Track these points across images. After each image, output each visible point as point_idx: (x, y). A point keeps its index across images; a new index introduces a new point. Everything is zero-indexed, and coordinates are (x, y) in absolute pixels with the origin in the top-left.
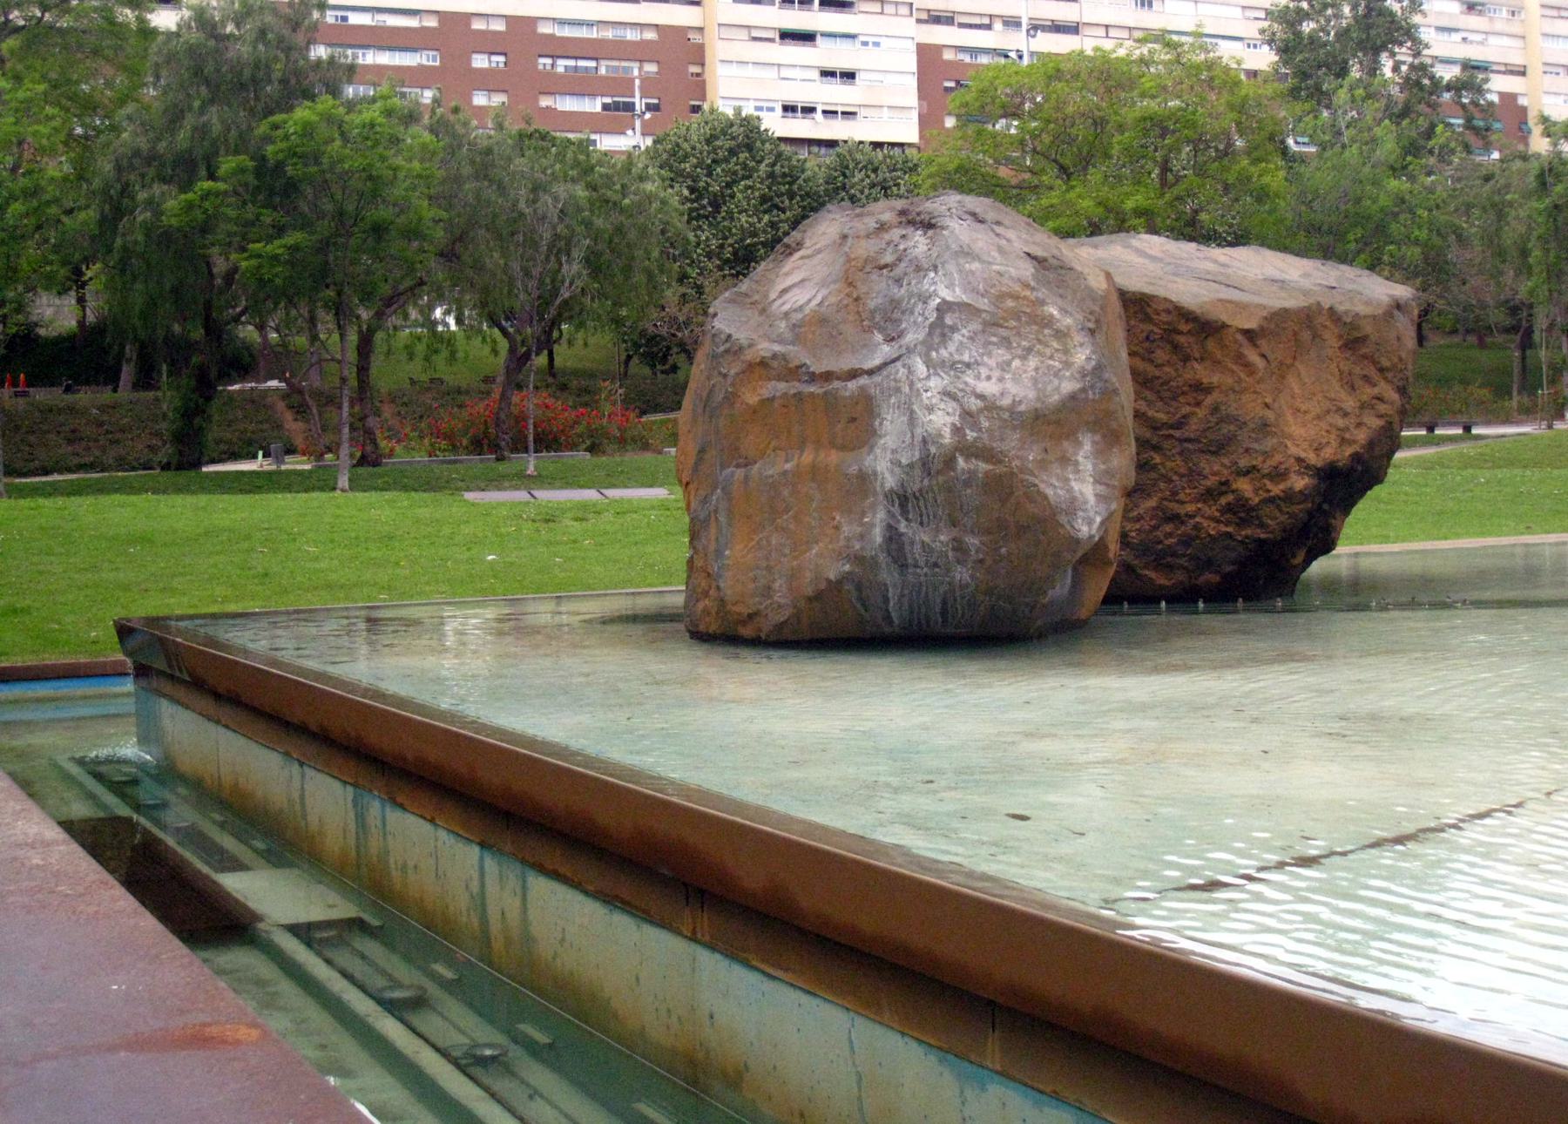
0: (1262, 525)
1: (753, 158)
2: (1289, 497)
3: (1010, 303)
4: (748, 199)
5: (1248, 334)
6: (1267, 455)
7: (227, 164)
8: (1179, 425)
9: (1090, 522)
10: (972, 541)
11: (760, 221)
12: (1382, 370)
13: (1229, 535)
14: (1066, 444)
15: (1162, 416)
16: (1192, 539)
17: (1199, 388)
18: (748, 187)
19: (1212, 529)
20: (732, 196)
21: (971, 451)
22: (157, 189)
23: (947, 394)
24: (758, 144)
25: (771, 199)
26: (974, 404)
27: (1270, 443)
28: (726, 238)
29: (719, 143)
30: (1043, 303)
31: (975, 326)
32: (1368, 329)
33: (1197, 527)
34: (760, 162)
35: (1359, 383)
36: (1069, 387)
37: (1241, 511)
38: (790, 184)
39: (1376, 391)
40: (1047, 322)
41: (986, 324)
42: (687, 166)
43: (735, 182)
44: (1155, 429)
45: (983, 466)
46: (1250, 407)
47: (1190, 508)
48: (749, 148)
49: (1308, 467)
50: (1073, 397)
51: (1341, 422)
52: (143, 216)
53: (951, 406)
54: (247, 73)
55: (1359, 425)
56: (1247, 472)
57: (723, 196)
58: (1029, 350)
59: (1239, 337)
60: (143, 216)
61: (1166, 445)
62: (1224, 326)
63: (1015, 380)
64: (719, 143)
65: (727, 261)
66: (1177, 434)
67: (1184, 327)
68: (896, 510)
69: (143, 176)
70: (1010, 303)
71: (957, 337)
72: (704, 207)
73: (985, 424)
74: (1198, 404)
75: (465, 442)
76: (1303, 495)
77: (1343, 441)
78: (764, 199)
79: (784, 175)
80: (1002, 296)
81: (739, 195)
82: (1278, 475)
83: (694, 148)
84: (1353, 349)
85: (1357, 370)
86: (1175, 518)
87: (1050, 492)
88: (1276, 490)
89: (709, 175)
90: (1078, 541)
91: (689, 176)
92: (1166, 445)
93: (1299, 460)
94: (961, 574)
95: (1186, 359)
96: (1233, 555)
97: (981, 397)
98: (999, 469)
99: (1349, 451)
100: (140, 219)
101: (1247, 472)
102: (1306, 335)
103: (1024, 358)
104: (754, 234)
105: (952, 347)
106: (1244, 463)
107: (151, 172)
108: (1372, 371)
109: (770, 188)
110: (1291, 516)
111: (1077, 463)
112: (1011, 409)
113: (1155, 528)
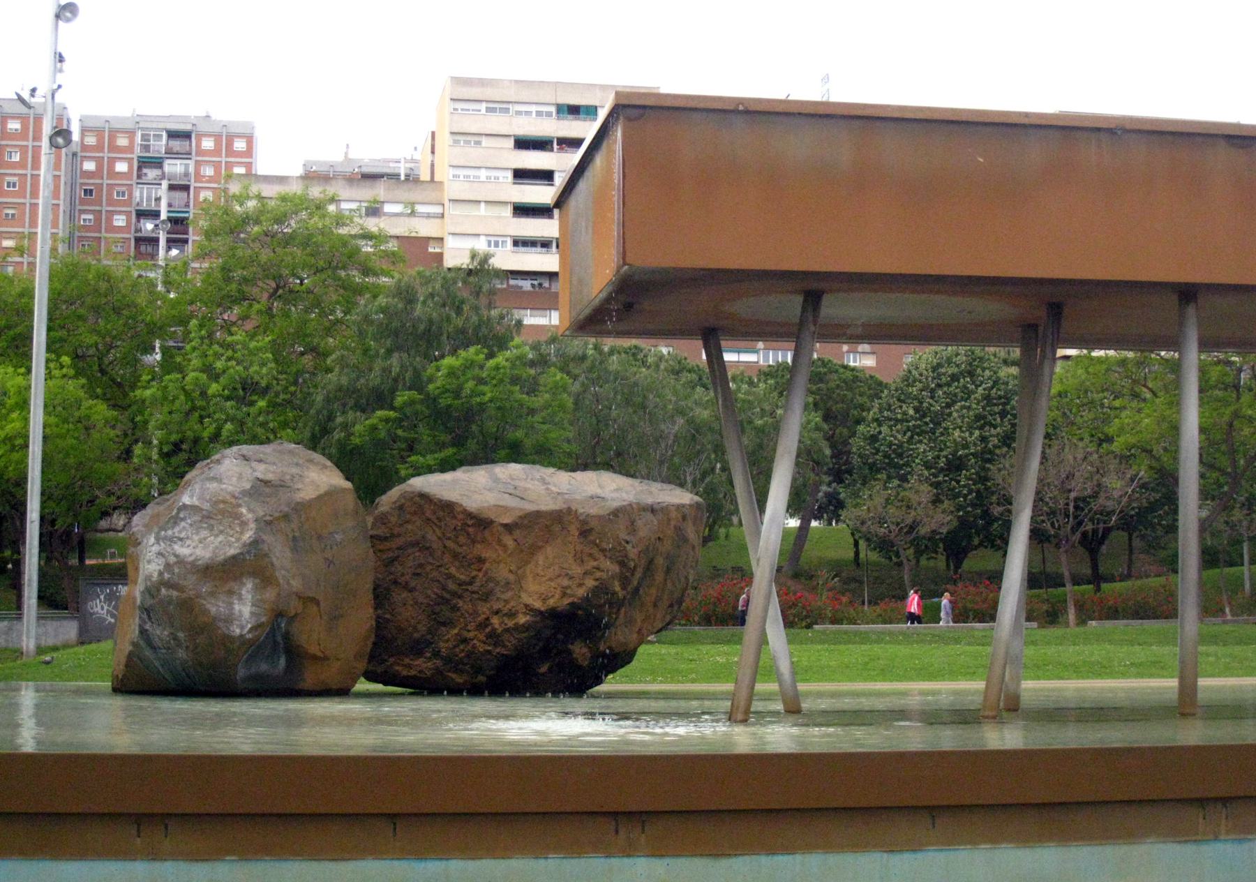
0: (504, 646)
1: (973, 383)
2: (517, 628)
3: (222, 506)
4: (963, 417)
5: (506, 526)
6: (506, 601)
7: (401, 398)
8: (471, 583)
9: (242, 628)
10: (181, 635)
11: (971, 434)
12: (603, 550)
13: (489, 652)
14: (232, 584)
15: (462, 577)
16: (473, 653)
17: (481, 561)
18: (963, 407)
19: (481, 648)
20: (950, 414)
21: (169, 585)
22: (351, 415)
23: (160, 554)
24: (979, 371)
25: (984, 417)
26: (172, 559)
27: (509, 595)
28: (941, 450)
29: (943, 370)
30: (240, 506)
31: (197, 518)
32: (593, 524)
33: (474, 647)
34: (977, 387)
35: (586, 559)
36: (232, 551)
37: (494, 637)
38: (1004, 404)
39: (595, 564)
40: (238, 516)
41: (203, 517)
42: (914, 390)
43: (954, 402)
44: (460, 585)
45: (175, 593)
46: (502, 573)
47: (471, 635)
48: (971, 374)
49: (531, 610)
50: (234, 557)
51: (566, 582)
52: (338, 435)
53: (162, 561)
54: (422, 327)
55: (580, 585)
56: (497, 613)
57: (942, 414)
58: (221, 532)
59: (501, 529)
60: (338, 435)
61: (465, 594)
62: (492, 522)
63: (204, 548)
64: (943, 370)
65: (942, 469)
66: (469, 588)
67: (470, 522)
68: (145, 616)
69: (344, 405)
70: (222, 506)
71: (183, 524)
72: (926, 424)
73: (176, 570)
74: (480, 570)
75: (696, 619)
76: (526, 627)
77: (564, 595)
78: (978, 417)
79: (1000, 397)
80: (216, 503)
81: (955, 415)
82: (512, 614)
83: (921, 375)
84: (585, 537)
85: (587, 550)
86: (465, 641)
87: (213, 610)
88: (511, 624)
89: (932, 397)
90: (233, 638)
91: (916, 398)
92: (465, 594)
93: (526, 606)
94: (181, 654)
95: (474, 542)
96: (492, 664)
97: (176, 556)
98: (184, 596)
99: (566, 601)
100: (337, 437)
101: (497, 613)
102: (557, 528)
103: (216, 536)
104: (966, 446)
105: (177, 529)
106: (496, 607)
107: (351, 402)
108: (595, 551)
109: (984, 408)
110: (519, 640)
111: (240, 595)
112: (193, 563)
113: (455, 647)
